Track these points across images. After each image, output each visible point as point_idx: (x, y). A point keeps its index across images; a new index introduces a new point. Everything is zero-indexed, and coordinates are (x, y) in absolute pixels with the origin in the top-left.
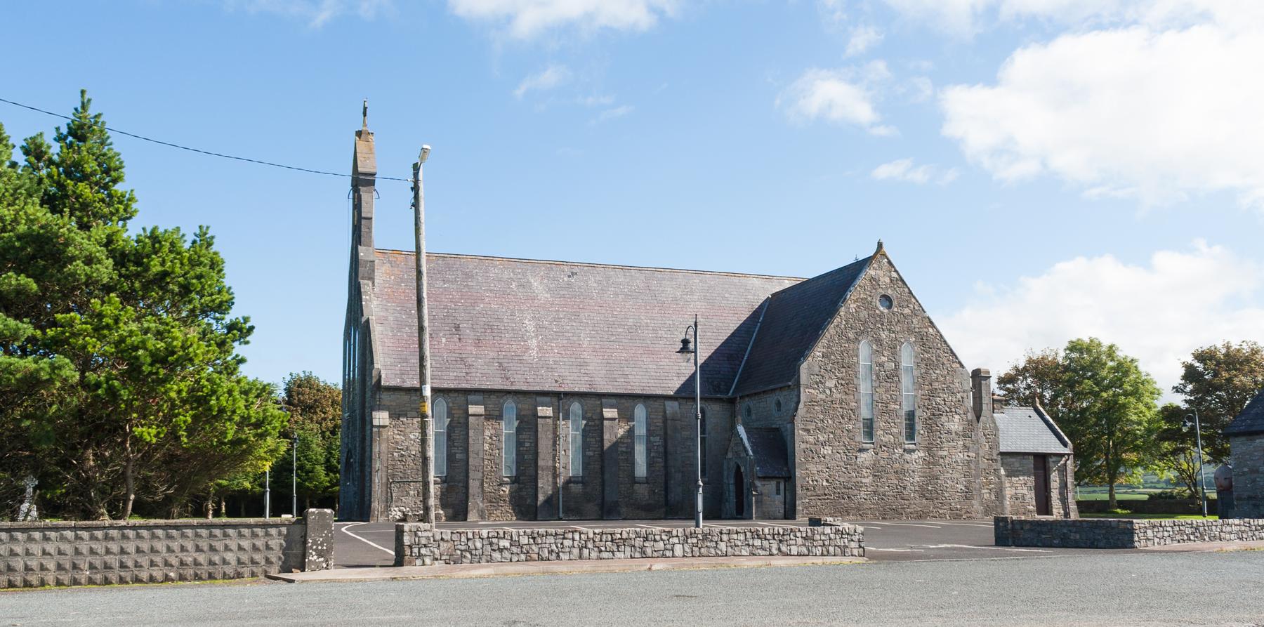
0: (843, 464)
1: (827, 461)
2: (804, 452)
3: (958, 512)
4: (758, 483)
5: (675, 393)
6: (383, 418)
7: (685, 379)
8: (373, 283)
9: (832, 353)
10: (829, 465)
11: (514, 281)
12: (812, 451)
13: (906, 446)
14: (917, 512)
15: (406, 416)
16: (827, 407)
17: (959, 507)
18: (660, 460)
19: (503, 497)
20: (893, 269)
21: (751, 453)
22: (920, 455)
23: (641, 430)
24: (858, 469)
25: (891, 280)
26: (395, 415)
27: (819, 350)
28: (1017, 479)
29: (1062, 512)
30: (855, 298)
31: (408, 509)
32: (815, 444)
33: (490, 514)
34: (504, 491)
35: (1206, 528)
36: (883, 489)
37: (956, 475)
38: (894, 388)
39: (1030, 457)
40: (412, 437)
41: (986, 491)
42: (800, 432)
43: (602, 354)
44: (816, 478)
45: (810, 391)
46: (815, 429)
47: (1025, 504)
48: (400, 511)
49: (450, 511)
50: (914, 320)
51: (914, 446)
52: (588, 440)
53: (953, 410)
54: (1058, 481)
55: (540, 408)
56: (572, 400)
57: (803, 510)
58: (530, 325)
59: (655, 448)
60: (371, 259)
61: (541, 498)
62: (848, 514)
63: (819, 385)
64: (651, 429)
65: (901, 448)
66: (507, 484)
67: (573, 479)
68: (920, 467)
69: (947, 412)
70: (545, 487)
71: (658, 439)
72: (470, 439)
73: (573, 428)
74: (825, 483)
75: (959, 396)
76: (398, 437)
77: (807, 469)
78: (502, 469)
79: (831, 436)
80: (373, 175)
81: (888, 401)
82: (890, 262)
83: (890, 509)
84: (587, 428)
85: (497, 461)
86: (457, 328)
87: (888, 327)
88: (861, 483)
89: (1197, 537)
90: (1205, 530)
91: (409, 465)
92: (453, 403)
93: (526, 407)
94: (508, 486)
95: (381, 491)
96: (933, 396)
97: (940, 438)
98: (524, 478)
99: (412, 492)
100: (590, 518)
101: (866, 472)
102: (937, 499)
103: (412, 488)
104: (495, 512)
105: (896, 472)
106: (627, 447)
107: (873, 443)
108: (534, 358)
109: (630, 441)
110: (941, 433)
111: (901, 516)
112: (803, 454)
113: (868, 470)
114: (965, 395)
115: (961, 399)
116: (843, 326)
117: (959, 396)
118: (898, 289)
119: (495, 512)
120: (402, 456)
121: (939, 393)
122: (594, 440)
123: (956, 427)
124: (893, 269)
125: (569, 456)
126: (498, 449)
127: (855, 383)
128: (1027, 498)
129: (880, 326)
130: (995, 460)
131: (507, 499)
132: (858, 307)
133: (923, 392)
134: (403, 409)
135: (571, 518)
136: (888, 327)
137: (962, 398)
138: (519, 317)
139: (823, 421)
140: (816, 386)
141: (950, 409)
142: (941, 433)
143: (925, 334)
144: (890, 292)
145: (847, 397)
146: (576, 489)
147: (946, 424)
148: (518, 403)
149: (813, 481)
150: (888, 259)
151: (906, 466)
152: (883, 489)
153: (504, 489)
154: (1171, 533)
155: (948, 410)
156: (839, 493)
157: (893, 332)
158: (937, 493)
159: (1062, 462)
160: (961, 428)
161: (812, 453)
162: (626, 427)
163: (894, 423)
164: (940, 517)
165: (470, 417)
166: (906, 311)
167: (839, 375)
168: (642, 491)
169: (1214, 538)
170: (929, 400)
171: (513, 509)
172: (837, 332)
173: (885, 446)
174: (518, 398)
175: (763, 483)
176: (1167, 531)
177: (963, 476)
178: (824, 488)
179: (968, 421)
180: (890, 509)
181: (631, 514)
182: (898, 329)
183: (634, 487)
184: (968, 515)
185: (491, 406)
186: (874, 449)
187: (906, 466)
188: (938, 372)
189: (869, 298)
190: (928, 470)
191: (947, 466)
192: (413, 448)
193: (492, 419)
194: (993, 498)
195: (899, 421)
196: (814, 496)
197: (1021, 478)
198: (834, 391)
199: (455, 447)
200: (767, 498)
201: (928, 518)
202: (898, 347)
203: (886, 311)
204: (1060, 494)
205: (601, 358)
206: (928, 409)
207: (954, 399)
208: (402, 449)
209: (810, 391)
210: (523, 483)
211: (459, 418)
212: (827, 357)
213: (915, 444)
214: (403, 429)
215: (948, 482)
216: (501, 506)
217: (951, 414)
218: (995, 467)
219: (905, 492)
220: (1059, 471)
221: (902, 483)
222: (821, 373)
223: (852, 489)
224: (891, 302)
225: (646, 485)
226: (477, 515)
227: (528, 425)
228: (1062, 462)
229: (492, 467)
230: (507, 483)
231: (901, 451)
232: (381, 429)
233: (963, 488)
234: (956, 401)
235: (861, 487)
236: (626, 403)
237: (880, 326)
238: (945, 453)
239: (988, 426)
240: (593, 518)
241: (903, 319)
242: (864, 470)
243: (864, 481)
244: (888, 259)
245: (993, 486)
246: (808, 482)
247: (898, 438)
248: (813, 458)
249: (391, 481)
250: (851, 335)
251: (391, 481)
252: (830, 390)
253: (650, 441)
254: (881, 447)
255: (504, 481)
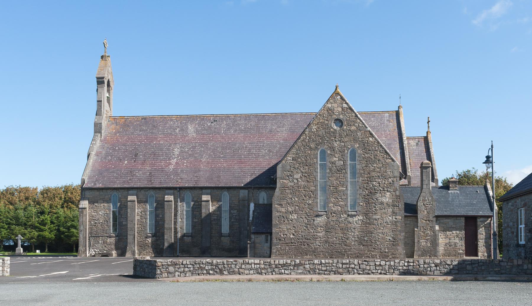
0: (304, 224)
1: (293, 223)
2: (279, 218)
3: (386, 254)
4: (253, 236)
5: (245, 185)
6: (84, 204)
7: (255, 177)
8: (101, 134)
9: (299, 158)
10: (295, 225)
11: (179, 128)
12: (283, 217)
13: (350, 213)
14: (355, 254)
15: (97, 202)
16: (295, 190)
17: (387, 250)
18: (237, 223)
19: (147, 244)
20: (344, 102)
21: (251, 219)
22: (359, 218)
23: (226, 208)
24: (315, 227)
25: (342, 109)
26: (91, 202)
27: (290, 156)
28: (451, 233)
29: (486, 254)
30: (316, 123)
31: (98, 250)
32: (286, 213)
33: (140, 253)
34: (148, 241)
35: (226, 266)
36: (332, 240)
37: (386, 231)
38: (342, 177)
39: (462, 218)
40: (101, 213)
41: (424, 241)
42: (276, 206)
43: (211, 165)
44: (286, 233)
45: (284, 181)
46: (286, 204)
47: (456, 249)
48: (94, 251)
49: (120, 251)
50: (358, 134)
51: (355, 213)
52: (195, 213)
53: (386, 189)
54: (484, 234)
55: (167, 196)
56: (186, 191)
57: (276, 252)
58: (177, 151)
59: (234, 216)
60: (100, 122)
61: (166, 245)
62: (307, 255)
63: (290, 177)
64: (232, 206)
65: (346, 214)
66: (150, 237)
67: (186, 235)
68: (359, 226)
69: (381, 190)
70: (169, 238)
71: (235, 211)
72: (128, 214)
73: (186, 206)
74: (292, 236)
75: (390, 180)
76: (93, 213)
77: (280, 228)
78: (147, 229)
79: (297, 208)
80: (103, 78)
81: (338, 185)
82: (342, 98)
83: (336, 252)
84: (195, 206)
85: (145, 225)
86: (136, 155)
87: (339, 139)
88: (317, 236)
89: (216, 272)
90: (224, 267)
91: (99, 228)
92: (121, 195)
93: (160, 196)
94: (151, 239)
95: (83, 241)
96: (371, 181)
97: (375, 207)
98: (159, 234)
99: (100, 242)
100: (195, 255)
101: (321, 229)
102: (371, 246)
103: (100, 239)
104: (143, 252)
105: (342, 229)
106: (217, 217)
107: (326, 212)
108: (171, 169)
109: (219, 213)
110: (375, 204)
111: (344, 256)
112: (278, 219)
113: (322, 228)
114: (395, 179)
115: (392, 182)
116: (307, 140)
117: (390, 180)
118: (347, 114)
119: (143, 252)
120: (96, 223)
121: (375, 179)
122: (198, 213)
123: (387, 200)
124: (344, 102)
125: (184, 222)
126: (145, 219)
127: (314, 175)
128: (458, 245)
129: (333, 139)
130: (431, 220)
131: (150, 245)
132: (318, 128)
133: (363, 179)
134: (96, 199)
135: (184, 256)
136: (339, 139)
137: (393, 181)
138: (173, 147)
139: (291, 199)
140: (287, 178)
141: (383, 188)
142: (375, 204)
143: (366, 142)
144: (341, 117)
145: (309, 184)
146: (188, 240)
147: (380, 198)
148: (156, 194)
149: (283, 235)
150: (340, 96)
151: (349, 225)
152: (332, 240)
153: (148, 240)
154: (192, 269)
155: (382, 189)
156: (301, 242)
157: (343, 142)
158: (371, 242)
159: (488, 221)
160: (391, 201)
161: (284, 218)
162: (217, 206)
163: (342, 199)
164: (372, 257)
165: (128, 202)
166: (353, 128)
167: (303, 171)
168: (226, 241)
169: (234, 273)
170: (368, 183)
171: (153, 251)
172: (303, 144)
173: (334, 213)
174: (156, 191)
175: (256, 236)
176: (188, 267)
177: (391, 231)
178: (291, 239)
179: (396, 196)
180: (336, 252)
181: (219, 254)
182: (346, 139)
183: (221, 239)
184: (394, 256)
185: (141, 196)
186: (326, 215)
187: (349, 225)
188: (375, 165)
189: (326, 122)
190: (365, 228)
191: (379, 225)
192: (101, 219)
193: (142, 203)
194: (429, 245)
195: (345, 197)
196: (283, 244)
197: (454, 232)
198: (300, 180)
199: (122, 218)
200: (259, 245)
201: (363, 257)
202: (346, 151)
203: (339, 129)
204: (485, 242)
205: (210, 167)
206: (366, 189)
207: (386, 183)
208: (96, 220)
209: (284, 181)
210: (158, 237)
211: (124, 203)
212: (296, 160)
213: (356, 212)
214: (96, 210)
215: (380, 235)
216: (147, 249)
217: (383, 192)
218: (431, 225)
219: (348, 242)
220: (485, 227)
221: (346, 236)
222: (291, 170)
223: (310, 239)
224: (342, 123)
225: (229, 237)
226: (131, 253)
227: (160, 206)
228: (488, 221)
229: (142, 229)
230: (150, 237)
231: (346, 216)
232: (83, 210)
233: (391, 239)
234: (388, 184)
235: (317, 238)
236: (217, 192)
237: (333, 139)
238: (378, 217)
239: (427, 199)
240: (197, 255)
241: (350, 133)
242: (319, 228)
243: (319, 234)
244: (340, 96)
245: (429, 237)
246: (280, 235)
247: (344, 208)
248: (284, 221)
249: (90, 236)
250: (313, 146)
251: (90, 236)
252: (297, 180)
253: (231, 213)
254: (331, 214)
255: (148, 236)
